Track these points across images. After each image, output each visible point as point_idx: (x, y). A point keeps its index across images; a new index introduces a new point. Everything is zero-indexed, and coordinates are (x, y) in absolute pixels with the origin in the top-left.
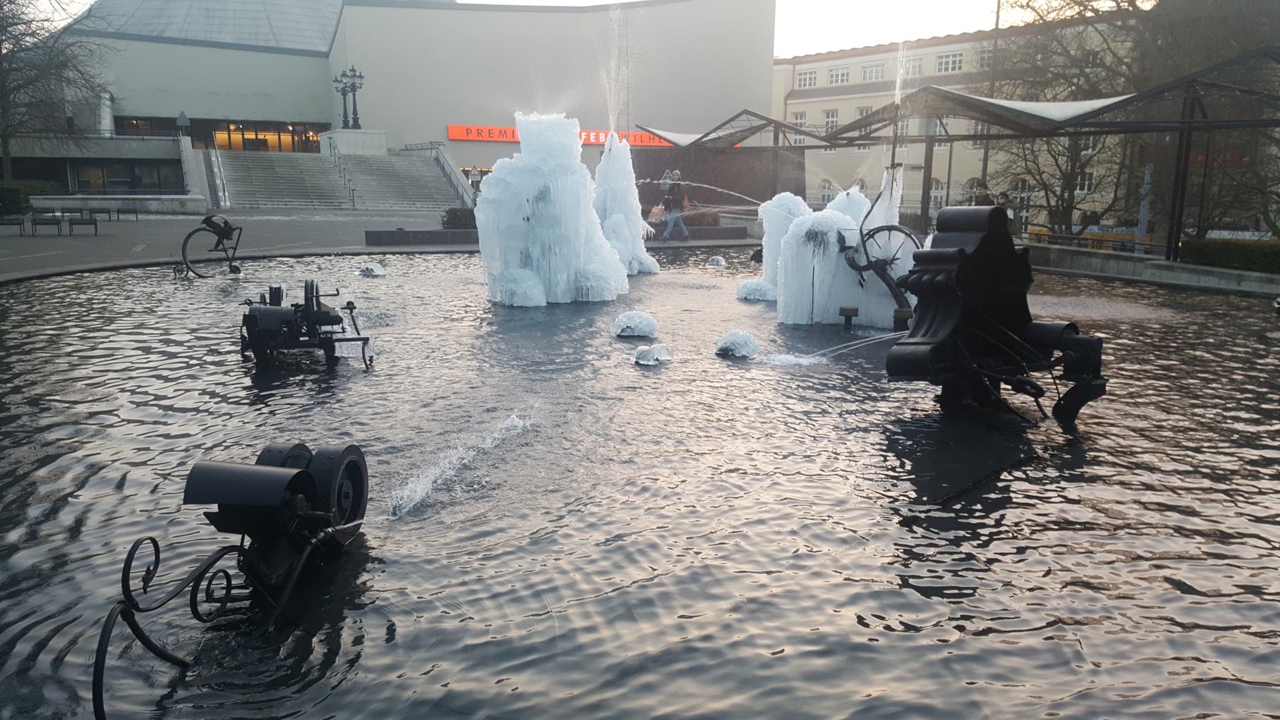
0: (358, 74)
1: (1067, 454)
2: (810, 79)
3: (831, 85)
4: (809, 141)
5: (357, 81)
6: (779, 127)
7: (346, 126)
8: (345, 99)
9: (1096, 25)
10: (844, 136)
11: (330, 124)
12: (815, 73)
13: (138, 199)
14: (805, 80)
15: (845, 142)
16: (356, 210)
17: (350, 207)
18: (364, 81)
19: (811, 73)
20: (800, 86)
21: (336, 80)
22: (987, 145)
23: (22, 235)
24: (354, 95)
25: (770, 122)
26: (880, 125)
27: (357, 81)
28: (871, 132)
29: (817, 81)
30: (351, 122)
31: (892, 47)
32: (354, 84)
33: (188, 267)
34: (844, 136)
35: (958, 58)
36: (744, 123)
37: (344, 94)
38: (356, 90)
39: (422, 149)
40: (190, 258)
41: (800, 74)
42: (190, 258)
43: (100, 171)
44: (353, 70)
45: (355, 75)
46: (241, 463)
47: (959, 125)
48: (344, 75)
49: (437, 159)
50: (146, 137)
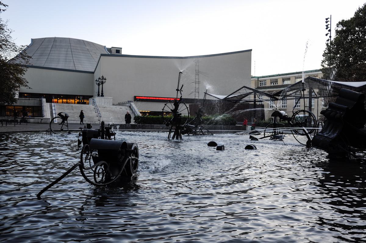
0: (104, 78)
2: (264, 83)
5: (104, 80)
7: (99, 95)
8: (99, 87)
12: (266, 81)
14: (262, 83)
18: (106, 81)
19: (264, 81)
20: (260, 85)
24: (102, 85)
27: (104, 80)
29: (266, 84)
30: (100, 94)
31: (301, 73)
32: (102, 81)
36: (244, 91)
37: (99, 85)
38: (103, 84)
41: (261, 81)
43: (206, 99)
44: (103, 77)
45: (103, 79)
46: (6, 177)
48: (99, 79)
50: (30, 99)
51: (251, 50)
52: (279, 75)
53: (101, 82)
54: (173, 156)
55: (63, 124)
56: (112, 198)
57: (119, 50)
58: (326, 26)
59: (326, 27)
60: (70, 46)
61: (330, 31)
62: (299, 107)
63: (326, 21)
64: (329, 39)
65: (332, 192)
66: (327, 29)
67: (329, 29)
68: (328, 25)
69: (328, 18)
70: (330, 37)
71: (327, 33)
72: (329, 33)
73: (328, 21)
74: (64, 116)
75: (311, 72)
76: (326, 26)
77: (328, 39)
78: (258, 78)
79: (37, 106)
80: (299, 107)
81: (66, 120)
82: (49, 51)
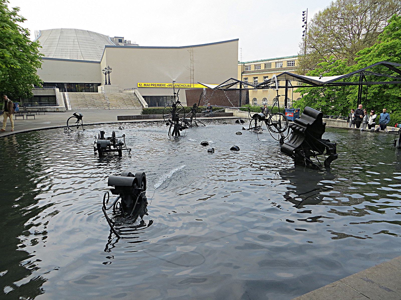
1: (17, 198)
2: (249, 68)
4: (249, 87)
6: (241, 83)
8: (106, 76)
10: (261, 86)
13: (44, 108)
15: (261, 88)
16: (110, 109)
17: (108, 109)
20: (246, 70)
21: (103, 70)
23: (24, 119)
25: (238, 81)
26: (224, 85)
27: (110, 70)
28: (268, 85)
30: (108, 83)
33: (69, 128)
34: (261, 86)
35: (293, 62)
36: (231, 82)
37: (106, 74)
38: (106, 74)
40: (69, 125)
42: (69, 125)
47: (294, 83)
51: (238, 40)
52: (262, 61)
55: (79, 122)
59: (303, 19)
60: (77, 36)
61: (306, 23)
63: (303, 13)
64: (305, 31)
66: (303, 21)
67: (305, 21)
70: (306, 29)
72: (305, 24)
74: (79, 115)
75: (289, 58)
78: (244, 63)
81: (81, 119)
82: (58, 39)
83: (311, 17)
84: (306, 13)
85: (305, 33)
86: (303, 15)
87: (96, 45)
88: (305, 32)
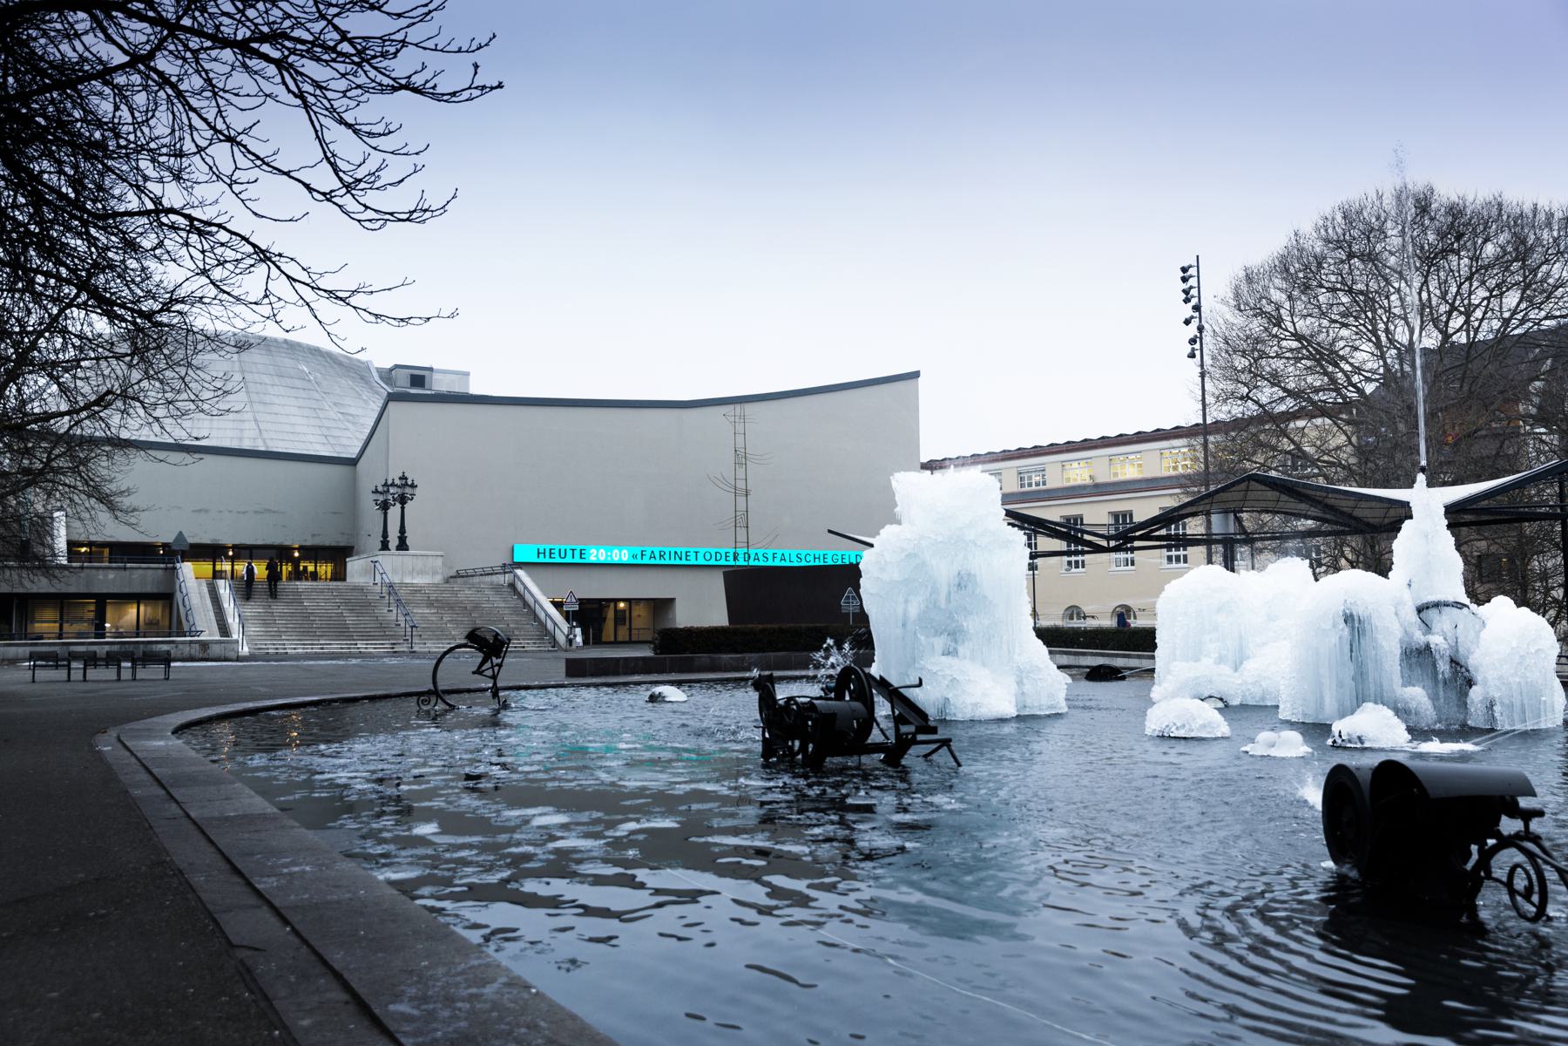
0: (409, 482)
3: (1023, 490)
9: (766, 878)
11: (352, 548)
13: (143, 642)
17: (406, 649)
18: (417, 491)
22: (62, 603)
24: (403, 508)
27: (408, 490)
30: (393, 541)
32: (403, 494)
37: (385, 506)
39: (467, 576)
44: (403, 478)
49: (512, 586)
50: (128, 565)
53: (399, 493)
54: (284, 766)
56: (1499, 956)
57: (423, 377)
58: (1184, 291)
61: (1197, 308)
62: (1083, 567)
63: (1182, 275)
64: (1196, 336)
65: (465, 889)
66: (1187, 301)
67: (1194, 301)
68: (1191, 287)
69: (1190, 266)
70: (1201, 329)
71: (1188, 316)
72: (1197, 314)
73: (1191, 276)
76: (1184, 291)
77: (1192, 336)
79: (155, 590)
80: (1083, 567)
83: (1216, 289)
84: (1193, 271)
85: (1197, 346)
86: (1184, 280)
87: (317, 396)
88: (1198, 340)
